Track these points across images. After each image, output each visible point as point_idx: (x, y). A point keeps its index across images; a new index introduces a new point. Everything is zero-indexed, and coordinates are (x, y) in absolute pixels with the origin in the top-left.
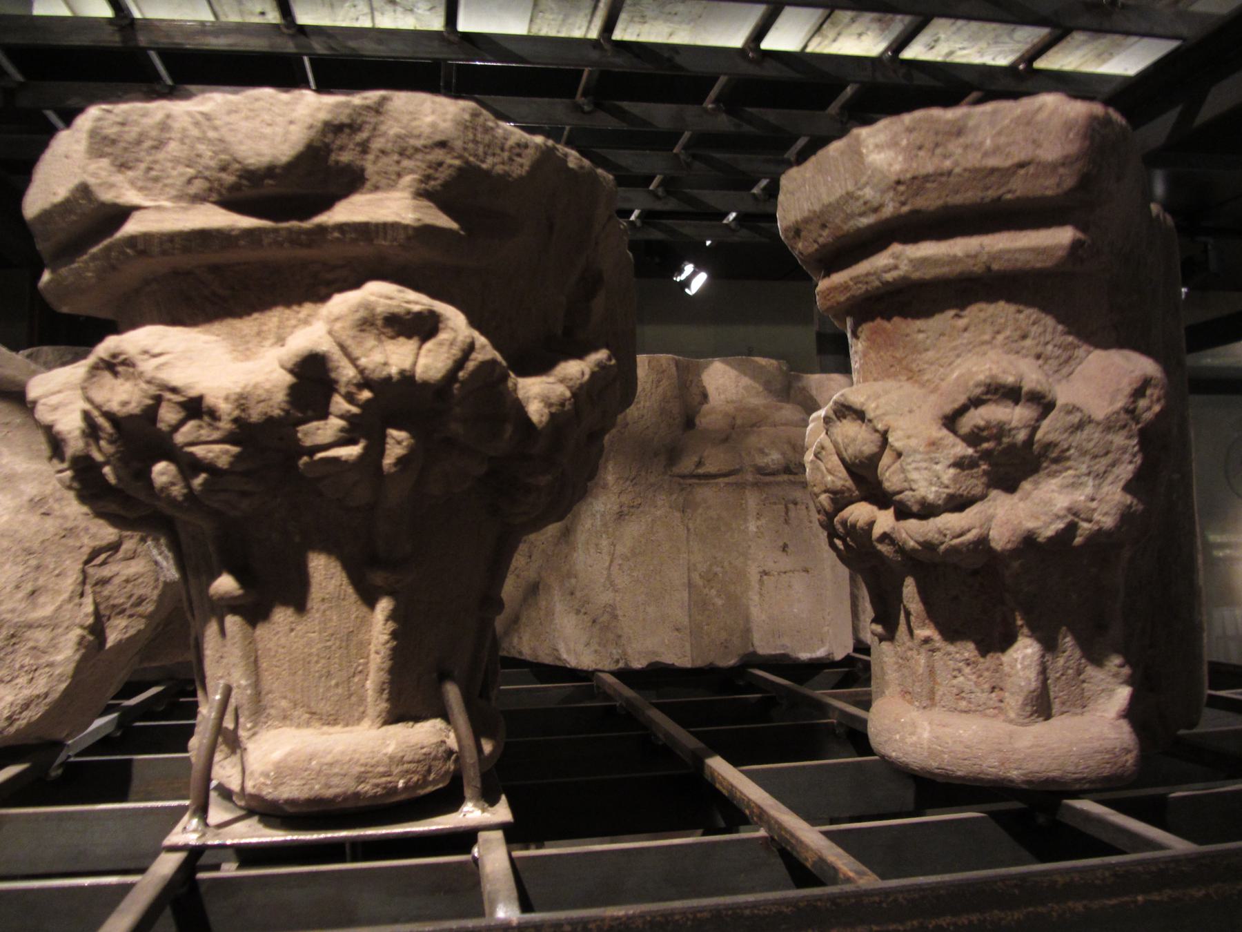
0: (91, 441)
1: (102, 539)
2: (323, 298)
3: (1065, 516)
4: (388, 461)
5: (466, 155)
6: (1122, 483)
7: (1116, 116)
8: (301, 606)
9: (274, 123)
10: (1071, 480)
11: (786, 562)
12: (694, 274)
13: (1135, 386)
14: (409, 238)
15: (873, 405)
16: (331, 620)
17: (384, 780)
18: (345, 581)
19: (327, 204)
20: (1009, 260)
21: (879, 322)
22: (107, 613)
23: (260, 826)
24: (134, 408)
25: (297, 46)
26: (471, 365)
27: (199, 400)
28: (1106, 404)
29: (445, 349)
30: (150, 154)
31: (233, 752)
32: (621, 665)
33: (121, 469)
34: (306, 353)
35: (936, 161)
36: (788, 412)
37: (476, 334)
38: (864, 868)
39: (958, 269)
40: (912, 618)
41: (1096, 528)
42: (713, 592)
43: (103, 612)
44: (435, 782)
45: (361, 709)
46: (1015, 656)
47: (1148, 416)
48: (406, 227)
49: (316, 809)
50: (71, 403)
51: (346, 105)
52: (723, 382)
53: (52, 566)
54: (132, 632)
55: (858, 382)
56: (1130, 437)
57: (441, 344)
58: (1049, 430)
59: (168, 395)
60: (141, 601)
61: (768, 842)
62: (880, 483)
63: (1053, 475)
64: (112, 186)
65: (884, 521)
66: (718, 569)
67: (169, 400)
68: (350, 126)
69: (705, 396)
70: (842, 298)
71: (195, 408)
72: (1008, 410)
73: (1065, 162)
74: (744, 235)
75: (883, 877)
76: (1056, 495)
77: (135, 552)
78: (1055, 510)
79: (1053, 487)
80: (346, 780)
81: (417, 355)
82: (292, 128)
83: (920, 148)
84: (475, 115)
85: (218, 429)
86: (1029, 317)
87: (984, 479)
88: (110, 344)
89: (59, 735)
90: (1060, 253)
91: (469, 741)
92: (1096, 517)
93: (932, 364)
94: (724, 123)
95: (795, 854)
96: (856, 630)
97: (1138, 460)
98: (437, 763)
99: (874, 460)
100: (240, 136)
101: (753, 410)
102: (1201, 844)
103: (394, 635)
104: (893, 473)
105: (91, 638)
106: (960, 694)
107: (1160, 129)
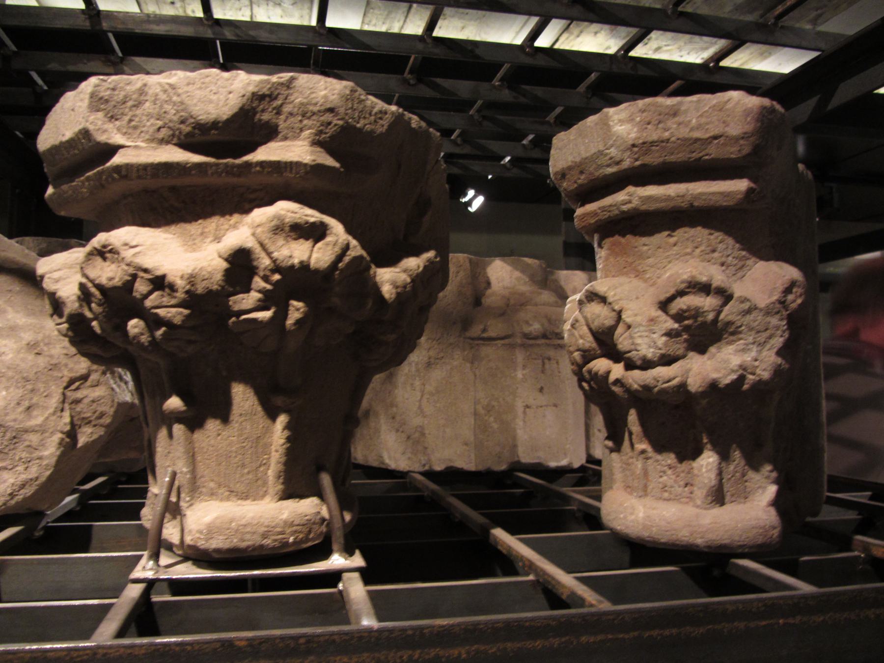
0: (84, 304)
1: (77, 372)
2: (248, 211)
3: (737, 371)
4: (290, 321)
5: (347, 118)
6: (775, 350)
7: (778, 107)
8: (224, 416)
9: (217, 91)
10: (742, 347)
11: (542, 399)
12: (474, 197)
13: (786, 286)
14: (307, 173)
15: (612, 293)
16: (246, 428)
17: (280, 536)
18: (256, 402)
19: (252, 147)
20: (705, 200)
21: (617, 238)
22: (79, 423)
23: (194, 567)
24: (117, 282)
25: (214, 33)
26: (347, 259)
27: (163, 277)
28: (766, 297)
29: (330, 247)
30: (130, 110)
31: (174, 518)
32: (427, 468)
33: (103, 326)
34: (237, 248)
35: (659, 131)
36: (546, 296)
37: (350, 238)
38: (602, 599)
39: (671, 204)
40: (634, 437)
41: (758, 379)
42: (492, 419)
43: (76, 422)
44: (313, 539)
45: (265, 489)
46: (702, 463)
47: (794, 306)
48: (306, 165)
49: (234, 556)
50: (68, 277)
51: (268, 82)
52: (501, 274)
53: (42, 390)
54: (95, 437)
55: (601, 278)
56: (781, 320)
57: (327, 244)
58: (729, 313)
59: (141, 274)
60: (102, 415)
61: (535, 584)
62: (615, 345)
63: (730, 343)
64: (105, 131)
65: (617, 371)
66: (495, 403)
67: (142, 277)
68: (270, 96)
69: (488, 284)
70: (593, 221)
71: (160, 283)
72: (702, 299)
73: (744, 136)
74: (515, 172)
75: (615, 602)
76: (732, 356)
77: (98, 381)
78: (731, 366)
79: (730, 351)
80: (255, 537)
81: (312, 251)
82: (231, 96)
83: (649, 124)
84: (353, 91)
85: (175, 297)
86: (717, 238)
87: (685, 345)
88: (101, 239)
89: (41, 507)
90: (740, 196)
91: (336, 512)
92: (758, 371)
93: (652, 267)
94: (506, 95)
95: (554, 590)
96: (588, 448)
97: (786, 335)
98: (314, 526)
99: (612, 329)
100: (195, 101)
101: (522, 294)
102: (820, 586)
103: (288, 439)
104: (625, 338)
105: (68, 440)
106: (664, 488)
107: (805, 110)
